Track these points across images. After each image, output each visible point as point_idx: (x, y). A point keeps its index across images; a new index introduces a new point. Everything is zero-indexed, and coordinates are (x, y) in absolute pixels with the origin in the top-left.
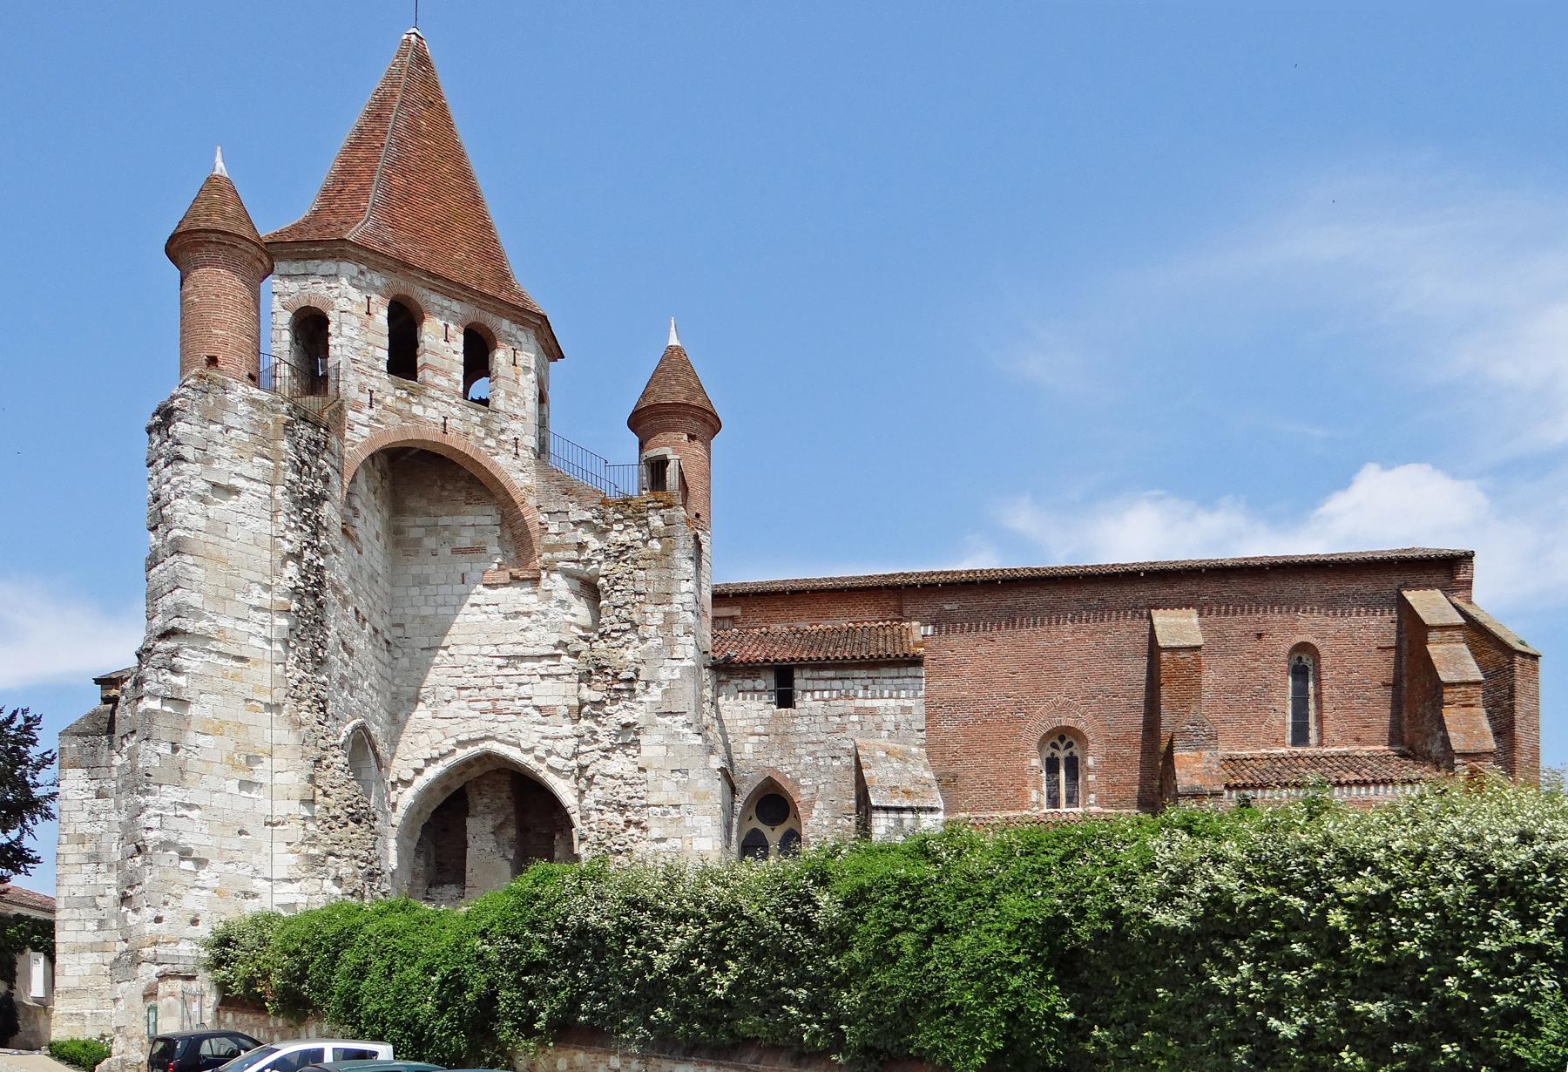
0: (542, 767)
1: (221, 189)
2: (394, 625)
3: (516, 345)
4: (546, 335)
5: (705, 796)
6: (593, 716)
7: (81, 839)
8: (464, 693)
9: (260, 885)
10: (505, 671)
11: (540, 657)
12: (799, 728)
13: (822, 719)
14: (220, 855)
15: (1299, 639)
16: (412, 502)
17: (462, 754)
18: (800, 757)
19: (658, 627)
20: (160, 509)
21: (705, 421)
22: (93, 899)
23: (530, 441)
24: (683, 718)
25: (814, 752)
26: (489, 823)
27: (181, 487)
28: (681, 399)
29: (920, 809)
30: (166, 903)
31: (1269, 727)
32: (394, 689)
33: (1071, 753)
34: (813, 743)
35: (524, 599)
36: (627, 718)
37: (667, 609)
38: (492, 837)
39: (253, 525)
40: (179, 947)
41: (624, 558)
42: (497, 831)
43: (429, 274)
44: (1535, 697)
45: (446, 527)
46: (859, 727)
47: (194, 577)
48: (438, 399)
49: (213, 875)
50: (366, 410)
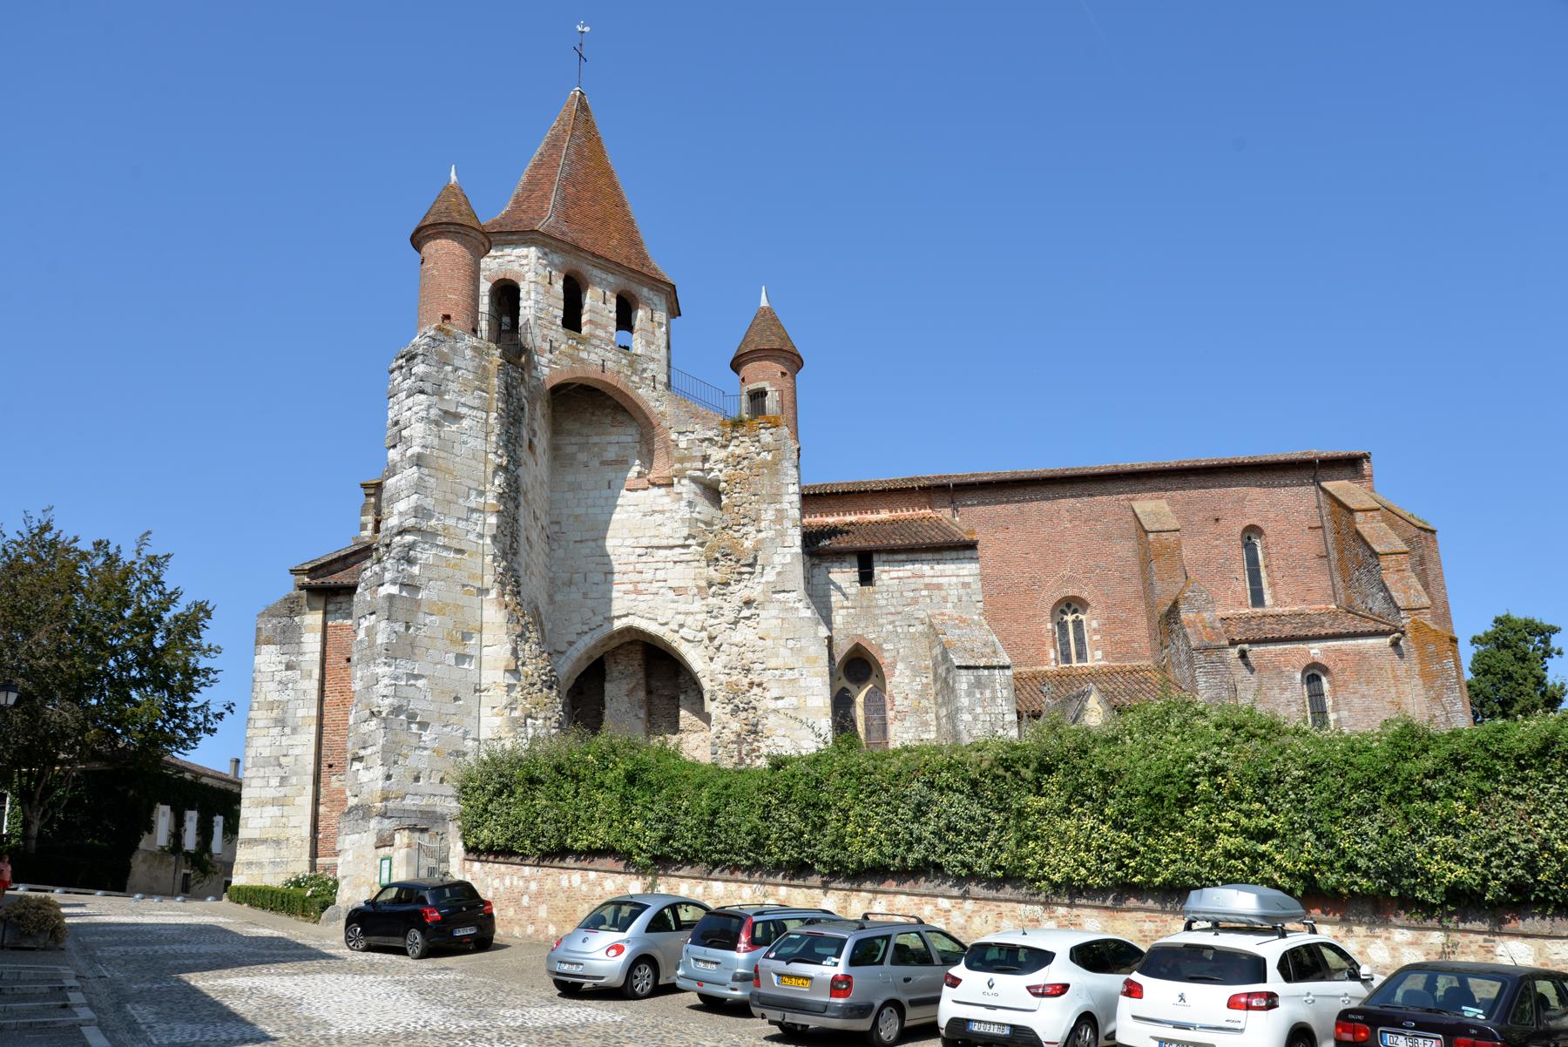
1: (456, 195)
2: (552, 523)
3: (653, 307)
4: (673, 300)
5: (815, 660)
7: (271, 706)
10: (644, 559)
11: (672, 547)
15: (1247, 522)
16: (569, 425)
18: (882, 626)
19: (771, 521)
21: (793, 362)
22: (277, 758)
23: (662, 378)
25: (894, 622)
26: (625, 686)
28: (776, 346)
29: (994, 667)
30: (395, 763)
31: (1234, 592)
32: (551, 575)
33: (1077, 617)
34: (892, 614)
36: (746, 594)
37: (778, 506)
38: (626, 699)
39: (472, 442)
41: (741, 466)
42: (630, 693)
43: (593, 254)
44: (1438, 563)
45: (595, 444)
46: (928, 600)
47: (428, 484)
48: (598, 346)
49: (434, 736)
50: (548, 355)
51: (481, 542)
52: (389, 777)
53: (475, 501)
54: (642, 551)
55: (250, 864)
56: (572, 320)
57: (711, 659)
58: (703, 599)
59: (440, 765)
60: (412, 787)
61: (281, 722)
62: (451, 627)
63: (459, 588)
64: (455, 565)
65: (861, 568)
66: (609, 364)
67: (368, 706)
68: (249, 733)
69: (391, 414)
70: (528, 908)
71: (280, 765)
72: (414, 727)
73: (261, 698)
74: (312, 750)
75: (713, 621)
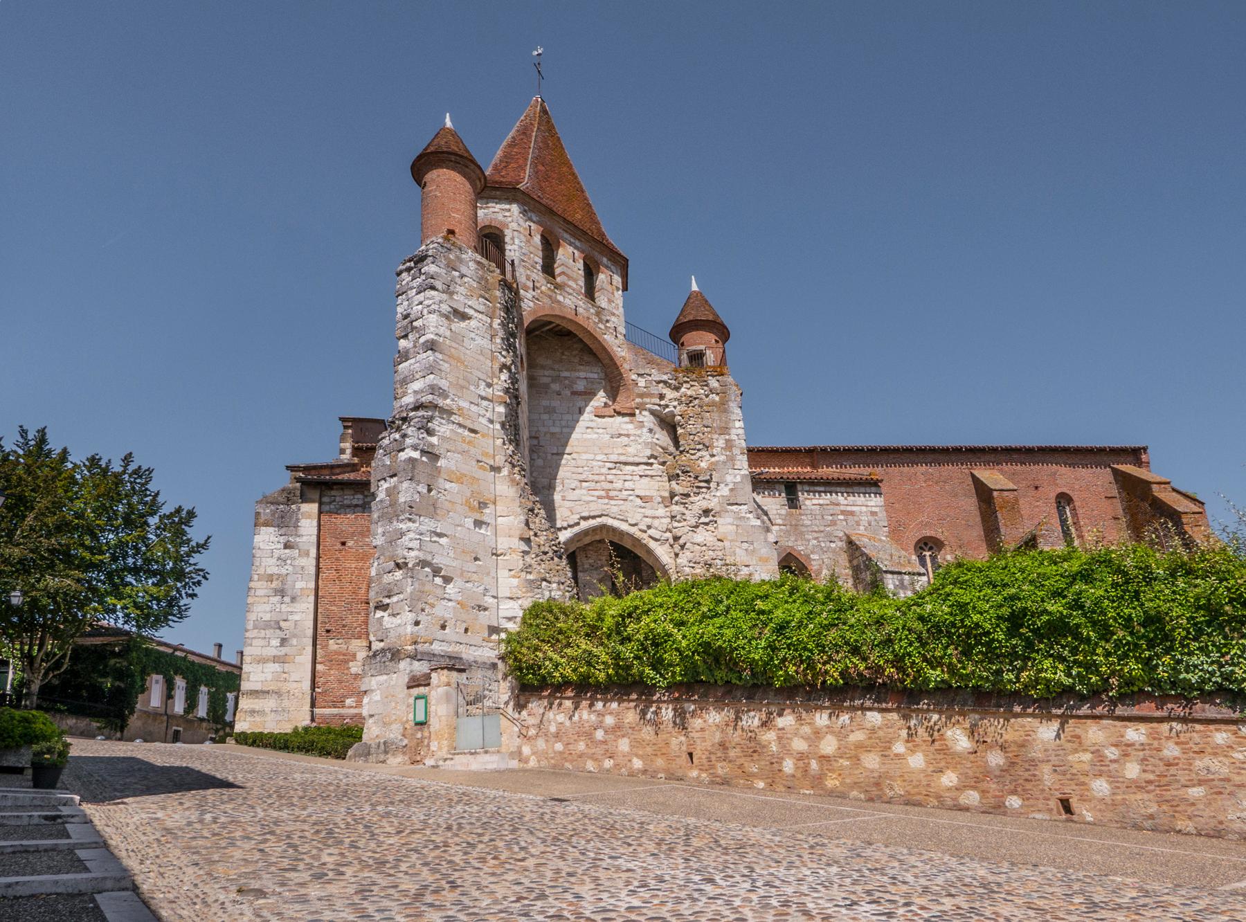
0: (645, 536)
6: (682, 503)
7: (270, 578)
8: (584, 484)
9: (489, 601)
10: (614, 471)
11: (638, 464)
12: (805, 522)
13: (819, 517)
14: (462, 575)
15: (1060, 490)
16: (541, 360)
17: (584, 525)
18: (809, 540)
20: (412, 322)
22: (278, 623)
24: (745, 507)
27: (433, 307)
30: (423, 610)
35: (624, 426)
36: (705, 504)
39: (479, 341)
40: (432, 647)
47: (443, 368)
49: (457, 590)
50: (531, 291)
51: (491, 426)
52: (417, 623)
53: (483, 390)
54: (611, 465)
55: (253, 712)
56: (548, 268)
57: (677, 555)
58: (666, 507)
59: (464, 617)
60: (440, 634)
61: (281, 592)
62: (469, 495)
63: (474, 463)
64: (469, 443)
65: (787, 494)
66: (580, 310)
67: (392, 558)
68: (250, 600)
69: (399, 309)
70: (605, 742)
71: (280, 628)
72: (438, 580)
73: (261, 571)
74: (311, 616)
75: (676, 524)
